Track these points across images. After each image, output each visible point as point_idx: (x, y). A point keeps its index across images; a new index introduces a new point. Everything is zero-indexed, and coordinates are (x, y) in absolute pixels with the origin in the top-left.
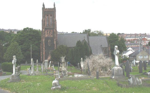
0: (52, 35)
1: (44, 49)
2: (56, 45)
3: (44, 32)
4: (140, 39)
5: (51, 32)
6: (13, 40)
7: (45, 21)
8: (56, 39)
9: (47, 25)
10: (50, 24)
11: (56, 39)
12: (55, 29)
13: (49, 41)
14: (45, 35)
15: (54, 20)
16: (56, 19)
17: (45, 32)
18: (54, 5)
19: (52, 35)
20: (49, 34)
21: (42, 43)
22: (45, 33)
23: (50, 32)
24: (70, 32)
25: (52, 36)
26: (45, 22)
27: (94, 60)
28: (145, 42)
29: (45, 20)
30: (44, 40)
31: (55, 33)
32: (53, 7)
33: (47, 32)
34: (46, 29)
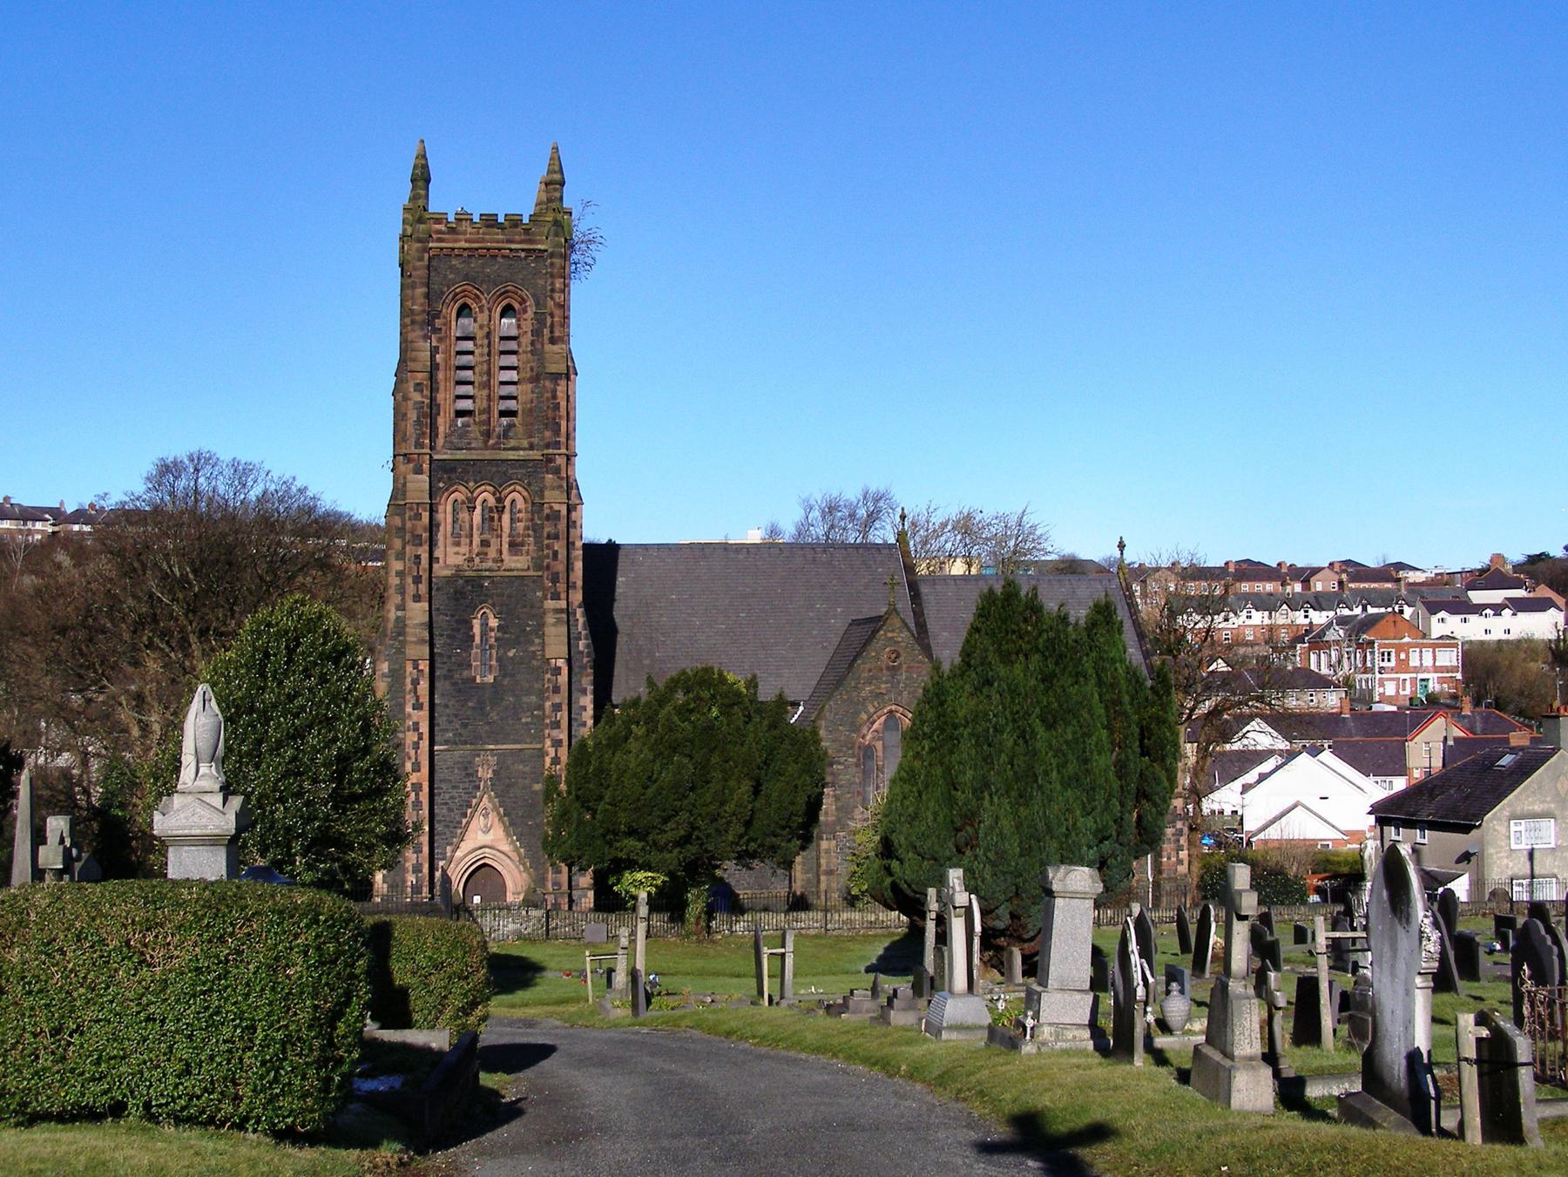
0: (515, 546)
1: (416, 727)
2: (563, 679)
3: (426, 516)
4: (1342, 621)
5: (506, 517)
6: (165, 566)
7: (441, 375)
8: (563, 604)
9: (453, 424)
10: (503, 414)
11: (563, 604)
12: (557, 471)
13: (485, 625)
14: (432, 544)
15: (552, 368)
16: (569, 356)
17: (432, 510)
18: (554, 183)
19: (515, 546)
20: (485, 543)
21: (400, 652)
22: (433, 527)
23: (492, 516)
24: (604, 541)
25: (518, 563)
26: (434, 389)
27: (265, 858)
28: (1403, 666)
29: (434, 367)
30: (418, 612)
31: (562, 525)
32: (522, 202)
33: (464, 515)
34: (445, 474)
